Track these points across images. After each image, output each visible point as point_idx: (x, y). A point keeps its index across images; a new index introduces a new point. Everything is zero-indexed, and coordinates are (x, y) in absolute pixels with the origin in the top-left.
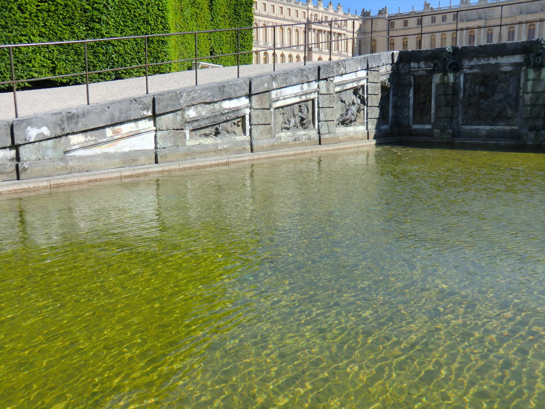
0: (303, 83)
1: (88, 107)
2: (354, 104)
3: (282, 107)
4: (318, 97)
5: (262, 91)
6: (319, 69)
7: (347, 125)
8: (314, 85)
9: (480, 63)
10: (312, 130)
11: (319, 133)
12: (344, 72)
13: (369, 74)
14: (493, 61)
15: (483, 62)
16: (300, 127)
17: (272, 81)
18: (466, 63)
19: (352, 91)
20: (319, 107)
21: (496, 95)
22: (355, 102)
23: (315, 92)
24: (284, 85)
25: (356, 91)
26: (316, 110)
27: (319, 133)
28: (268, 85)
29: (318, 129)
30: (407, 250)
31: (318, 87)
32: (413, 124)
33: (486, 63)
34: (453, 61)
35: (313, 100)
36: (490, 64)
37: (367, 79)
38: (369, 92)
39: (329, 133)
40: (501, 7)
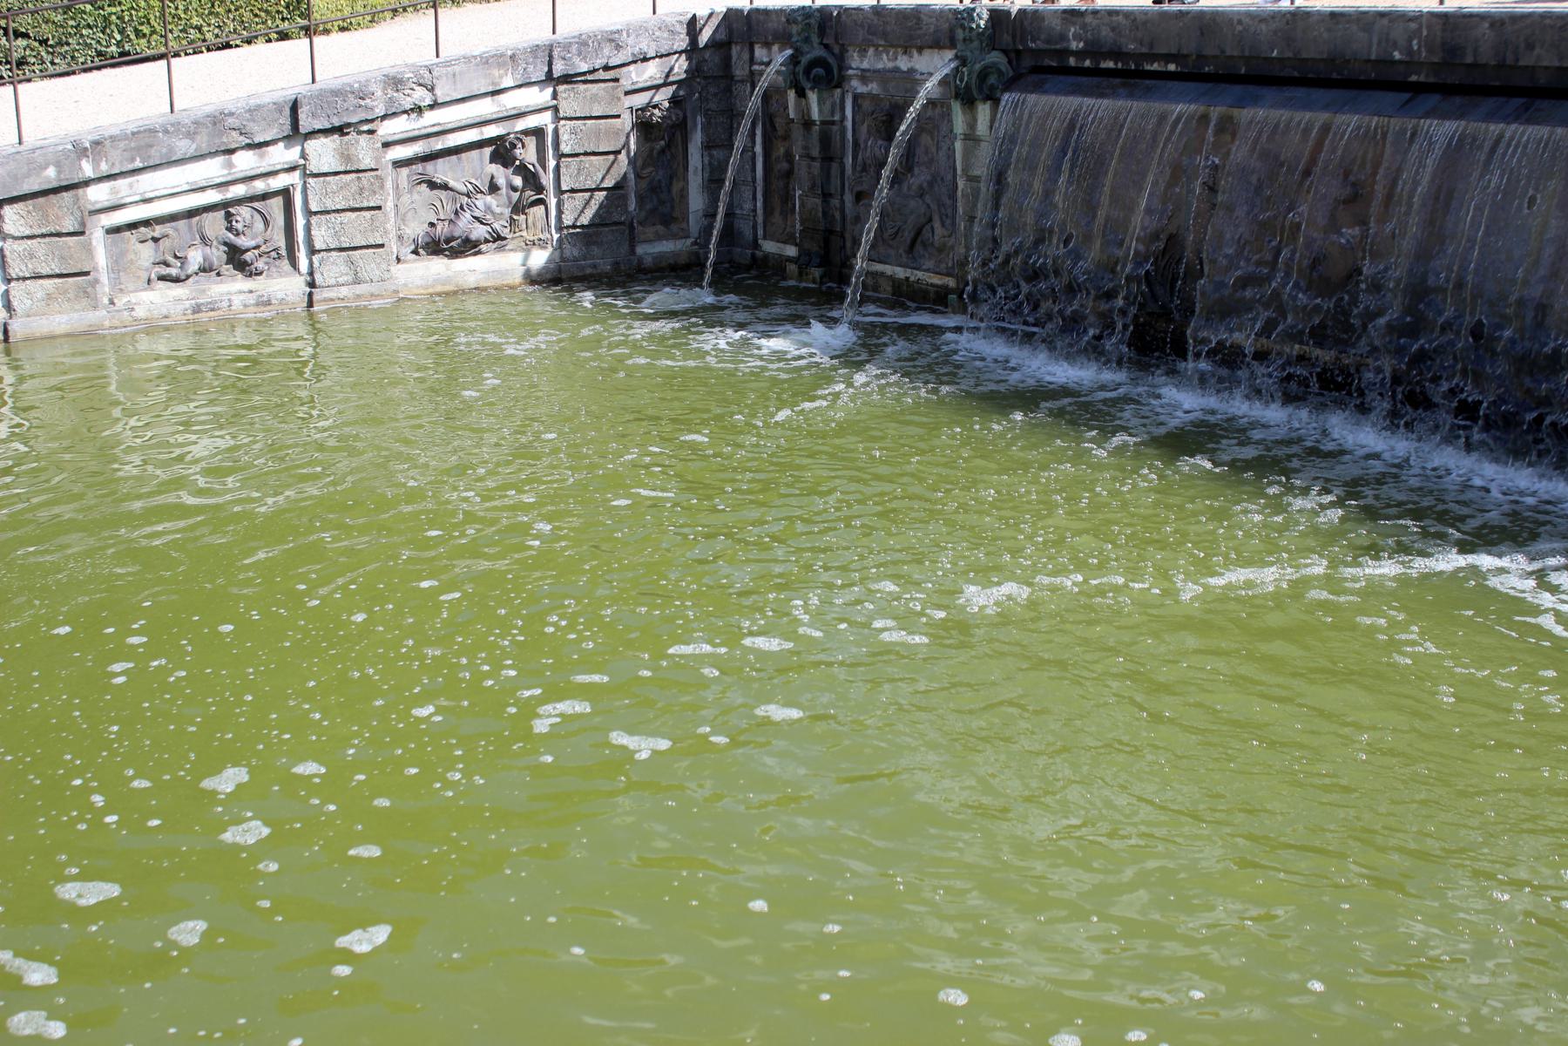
0: (231, 152)
1: (172, 118)
2: (493, 188)
3: (146, 223)
4: (556, 131)
5: (36, 188)
6: (295, 107)
7: (456, 253)
8: (282, 155)
9: (880, 66)
10: (287, 275)
11: (312, 284)
12: (428, 102)
13: (561, 95)
14: (903, 63)
15: (885, 63)
16: (228, 269)
17: (80, 160)
18: (858, 62)
19: (488, 151)
20: (309, 213)
21: (916, 170)
22: (501, 182)
23: (292, 169)
24: (138, 164)
25: (502, 152)
26: (300, 222)
27: (312, 284)
28: (59, 172)
29: (311, 274)
30: (1277, 648)
31: (304, 156)
32: (765, 238)
33: (890, 65)
34: (819, 52)
35: (286, 193)
36: (896, 70)
37: (556, 109)
38: (565, 149)
39: (357, 281)
40: (163, 63)
